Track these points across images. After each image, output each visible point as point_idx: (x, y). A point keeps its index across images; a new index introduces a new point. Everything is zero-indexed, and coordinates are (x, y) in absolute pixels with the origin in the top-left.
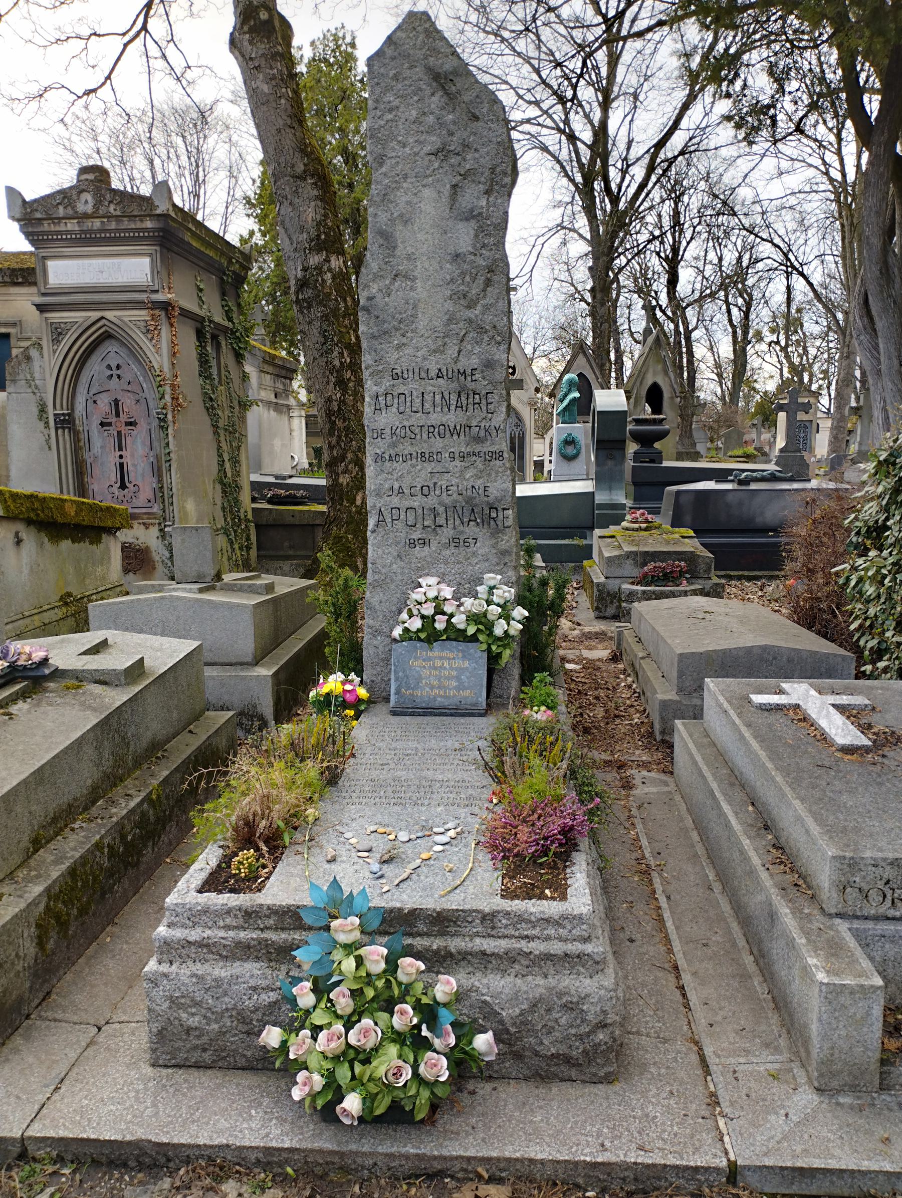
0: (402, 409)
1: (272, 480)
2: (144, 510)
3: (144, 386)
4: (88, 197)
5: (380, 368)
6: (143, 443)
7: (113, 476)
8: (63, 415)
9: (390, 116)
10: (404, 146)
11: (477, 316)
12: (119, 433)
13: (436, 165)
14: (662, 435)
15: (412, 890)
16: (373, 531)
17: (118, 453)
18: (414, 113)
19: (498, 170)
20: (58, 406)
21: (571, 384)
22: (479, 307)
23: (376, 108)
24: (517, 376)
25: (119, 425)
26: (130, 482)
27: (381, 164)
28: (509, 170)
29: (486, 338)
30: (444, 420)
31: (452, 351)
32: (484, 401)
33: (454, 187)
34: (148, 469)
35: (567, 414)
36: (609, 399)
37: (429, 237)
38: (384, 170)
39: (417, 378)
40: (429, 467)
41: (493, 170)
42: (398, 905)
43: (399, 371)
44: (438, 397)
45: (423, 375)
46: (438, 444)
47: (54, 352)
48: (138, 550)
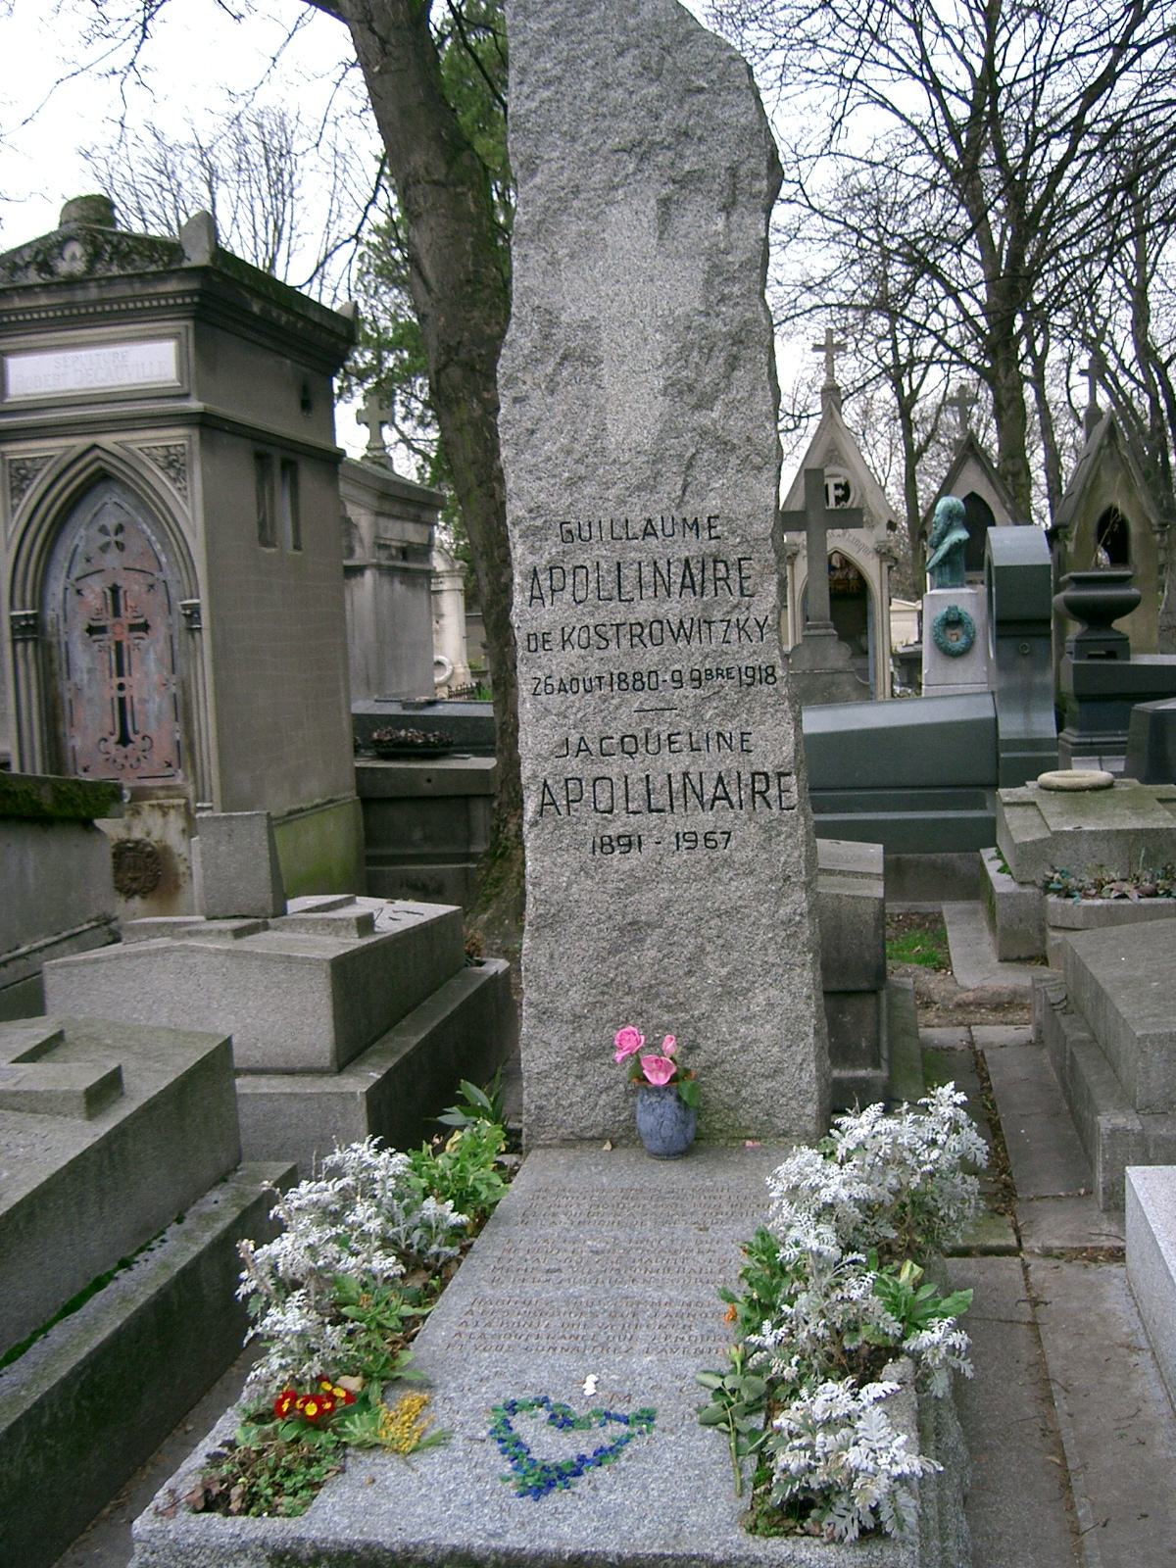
0: (581, 595)
1: (394, 709)
2: (160, 782)
3: (163, 559)
4: (75, 249)
5: (539, 522)
6: (159, 661)
7: (109, 722)
8: (26, 617)
9: (546, 94)
10: (573, 139)
11: (714, 422)
12: (119, 645)
13: (631, 167)
14: (1127, 606)
15: (583, 1517)
16: (534, 824)
17: (117, 681)
18: (588, 85)
19: (743, 170)
20: (17, 604)
21: (951, 516)
22: (718, 407)
23: (521, 83)
24: (853, 502)
25: (117, 628)
26: (136, 732)
27: (533, 173)
28: (763, 169)
29: (734, 461)
30: (661, 612)
31: (671, 485)
32: (734, 574)
33: (665, 202)
34: (167, 706)
35: (947, 570)
36: (1016, 543)
37: (624, 290)
38: (538, 180)
39: (607, 537)
40: (637, 700)
41: (733, 172)
42: (552, 1545)
43: (573, 526)
44: (647, 572)
45: (618, 531)
46: (649, 657)
47: (14, 509)
48: (150, 855)
